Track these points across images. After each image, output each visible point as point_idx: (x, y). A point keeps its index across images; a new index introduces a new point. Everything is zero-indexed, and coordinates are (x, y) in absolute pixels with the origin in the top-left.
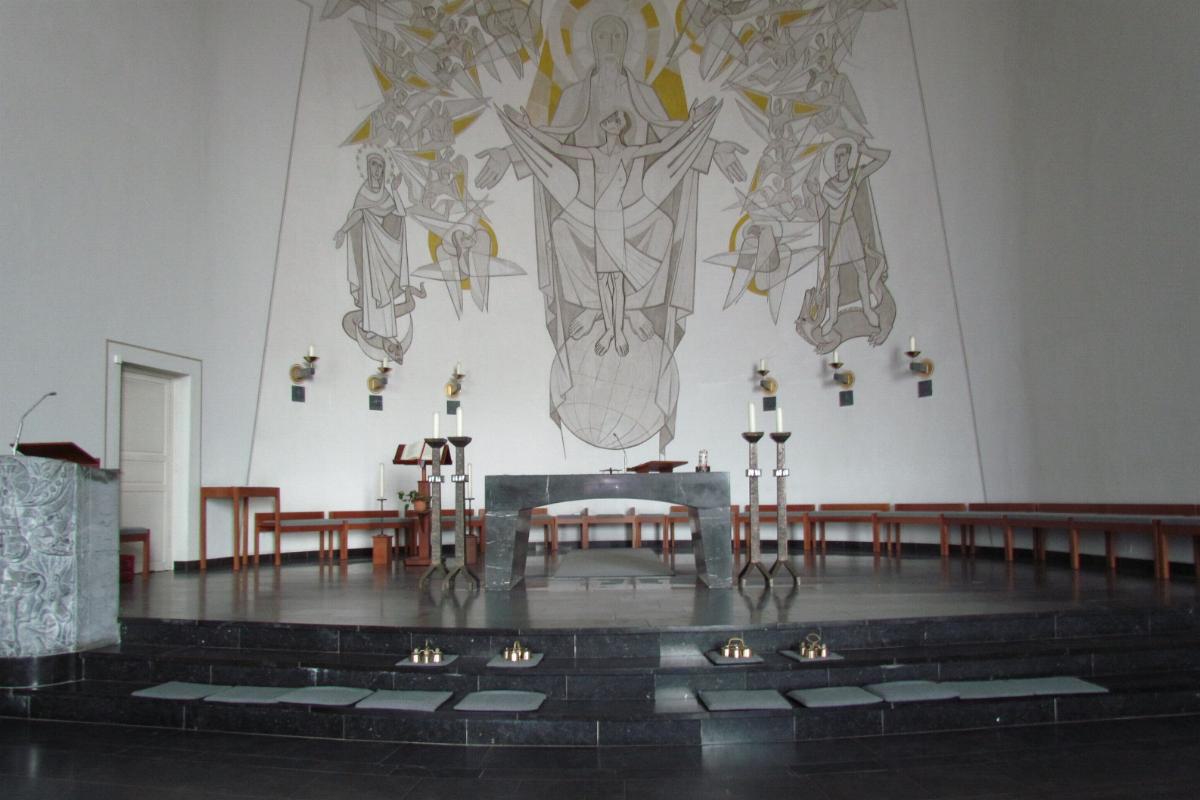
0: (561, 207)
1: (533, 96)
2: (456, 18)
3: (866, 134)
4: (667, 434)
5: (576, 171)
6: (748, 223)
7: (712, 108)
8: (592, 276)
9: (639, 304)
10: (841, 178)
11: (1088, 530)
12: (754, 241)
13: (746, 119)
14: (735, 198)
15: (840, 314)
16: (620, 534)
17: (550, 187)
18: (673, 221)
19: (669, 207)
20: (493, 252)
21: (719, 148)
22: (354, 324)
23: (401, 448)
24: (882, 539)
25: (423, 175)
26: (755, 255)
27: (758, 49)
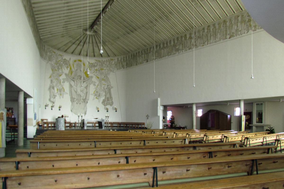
1: (69, 72)
2: (60, 62)
6: (96, 91)
7: (92, 77)
11: (131, 124)
15: (107, 103)
17: (71, 83)
19: (86, 87)
20: (64, 91)
27: (98, 72)
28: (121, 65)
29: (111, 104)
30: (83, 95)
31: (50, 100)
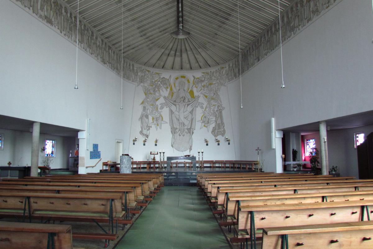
1: (169, 94)
2: (156, 82)
4: (191, 149)
6: (204, 116)
7: (199, 97)
11: (244, 164)
12: (205, 119)
16: (183, 165)
19: (191, 112)
21: (200, 103)
22: (141, 133)
23: (151, 152)
24: (223, 166)
25: (151, 108)
27: (206, 88)
28: (233, 74)
30: (187, 123)
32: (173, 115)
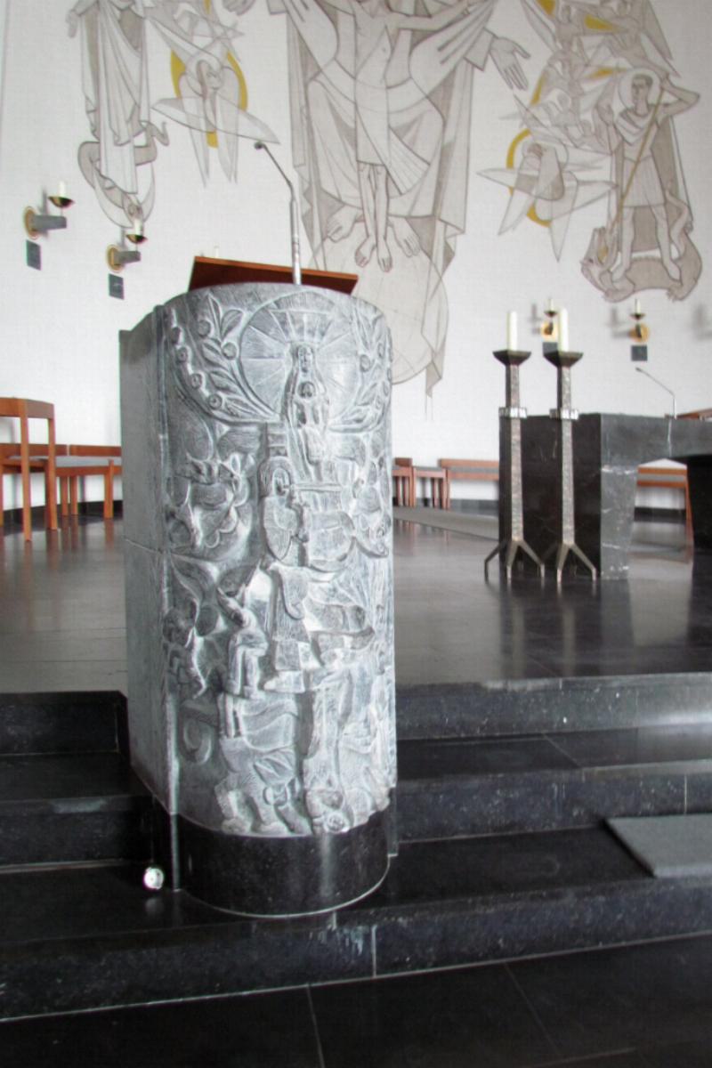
0: (319, 67)
3: (670, 70)
5: (334, 22)
8: (352, 164)
9: (404, 212)
10: (639, 112)
12: (534, 161)
13: (528, 17)
14: (514, 108)
15: (633, 262)
18: (443, 117)
19: (440, 97)
20: (242, 105)
21: (497, 44)
26: (537, 179)
29: (675, 273)
31: (90, 158)
32: (313, 86)
